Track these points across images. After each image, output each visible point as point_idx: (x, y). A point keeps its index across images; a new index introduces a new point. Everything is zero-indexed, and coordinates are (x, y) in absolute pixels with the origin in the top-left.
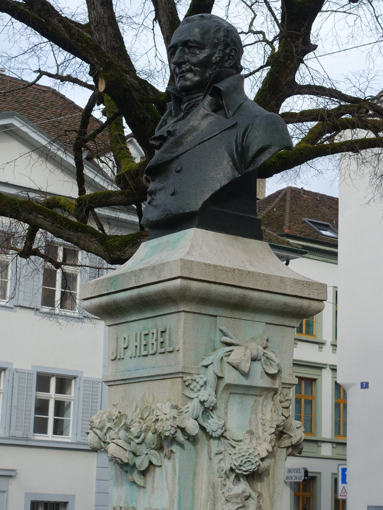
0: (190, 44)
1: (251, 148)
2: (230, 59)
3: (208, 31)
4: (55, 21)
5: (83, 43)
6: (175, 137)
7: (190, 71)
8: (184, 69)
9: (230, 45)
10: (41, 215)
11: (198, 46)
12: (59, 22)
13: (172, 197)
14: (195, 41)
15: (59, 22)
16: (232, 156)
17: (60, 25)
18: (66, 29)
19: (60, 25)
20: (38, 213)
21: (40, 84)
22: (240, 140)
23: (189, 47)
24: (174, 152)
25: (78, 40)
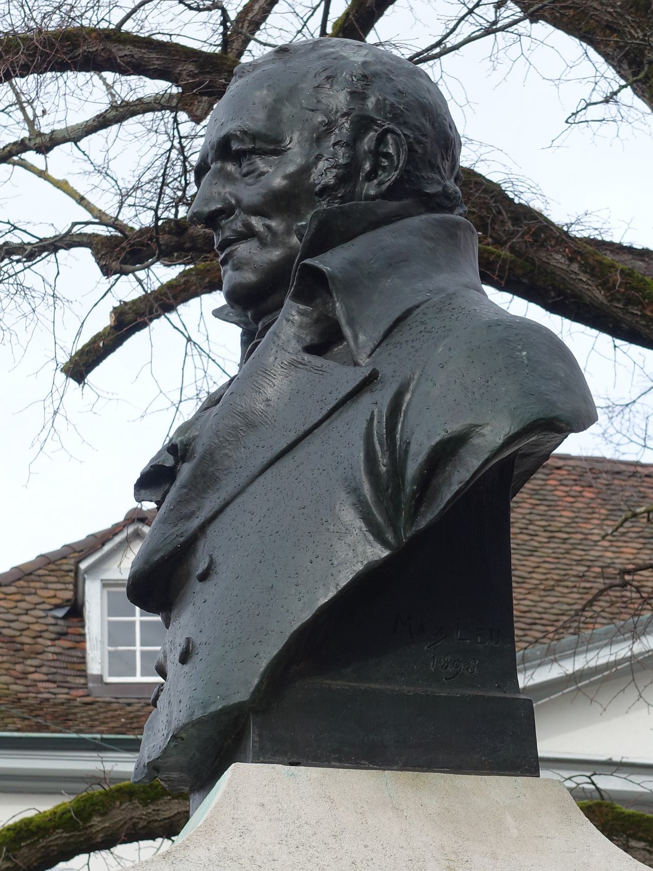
0: (235, 146)
1: (413, 448)
2: (384, 168)
3: (293, 91)
4: (558, 260)
5: (644, 308)
6: (194, 461)
7: (249, 234)
8: (227, 233)
9: (373, 121)
10: (640, 839)
11: (259, 145)
12: (571, 260)
13: (186, 668)
14: (244, 132)
15: (571, 260)
16: (355, 491)
17: (575, 267)
18: (593, 275)
19: (575, 267)
20: (629, 836)
21: (574, 453)
22: (379, 428)
23: (238, 157)
24: (193, 513)
25: (629, 301)
